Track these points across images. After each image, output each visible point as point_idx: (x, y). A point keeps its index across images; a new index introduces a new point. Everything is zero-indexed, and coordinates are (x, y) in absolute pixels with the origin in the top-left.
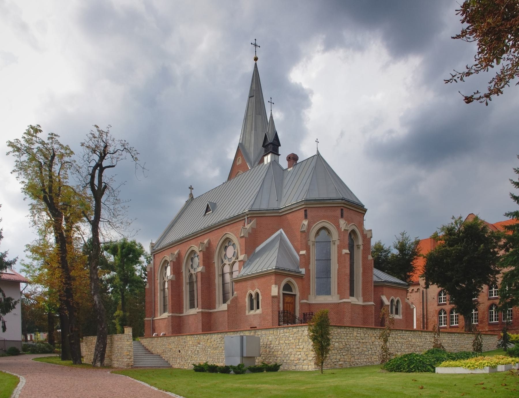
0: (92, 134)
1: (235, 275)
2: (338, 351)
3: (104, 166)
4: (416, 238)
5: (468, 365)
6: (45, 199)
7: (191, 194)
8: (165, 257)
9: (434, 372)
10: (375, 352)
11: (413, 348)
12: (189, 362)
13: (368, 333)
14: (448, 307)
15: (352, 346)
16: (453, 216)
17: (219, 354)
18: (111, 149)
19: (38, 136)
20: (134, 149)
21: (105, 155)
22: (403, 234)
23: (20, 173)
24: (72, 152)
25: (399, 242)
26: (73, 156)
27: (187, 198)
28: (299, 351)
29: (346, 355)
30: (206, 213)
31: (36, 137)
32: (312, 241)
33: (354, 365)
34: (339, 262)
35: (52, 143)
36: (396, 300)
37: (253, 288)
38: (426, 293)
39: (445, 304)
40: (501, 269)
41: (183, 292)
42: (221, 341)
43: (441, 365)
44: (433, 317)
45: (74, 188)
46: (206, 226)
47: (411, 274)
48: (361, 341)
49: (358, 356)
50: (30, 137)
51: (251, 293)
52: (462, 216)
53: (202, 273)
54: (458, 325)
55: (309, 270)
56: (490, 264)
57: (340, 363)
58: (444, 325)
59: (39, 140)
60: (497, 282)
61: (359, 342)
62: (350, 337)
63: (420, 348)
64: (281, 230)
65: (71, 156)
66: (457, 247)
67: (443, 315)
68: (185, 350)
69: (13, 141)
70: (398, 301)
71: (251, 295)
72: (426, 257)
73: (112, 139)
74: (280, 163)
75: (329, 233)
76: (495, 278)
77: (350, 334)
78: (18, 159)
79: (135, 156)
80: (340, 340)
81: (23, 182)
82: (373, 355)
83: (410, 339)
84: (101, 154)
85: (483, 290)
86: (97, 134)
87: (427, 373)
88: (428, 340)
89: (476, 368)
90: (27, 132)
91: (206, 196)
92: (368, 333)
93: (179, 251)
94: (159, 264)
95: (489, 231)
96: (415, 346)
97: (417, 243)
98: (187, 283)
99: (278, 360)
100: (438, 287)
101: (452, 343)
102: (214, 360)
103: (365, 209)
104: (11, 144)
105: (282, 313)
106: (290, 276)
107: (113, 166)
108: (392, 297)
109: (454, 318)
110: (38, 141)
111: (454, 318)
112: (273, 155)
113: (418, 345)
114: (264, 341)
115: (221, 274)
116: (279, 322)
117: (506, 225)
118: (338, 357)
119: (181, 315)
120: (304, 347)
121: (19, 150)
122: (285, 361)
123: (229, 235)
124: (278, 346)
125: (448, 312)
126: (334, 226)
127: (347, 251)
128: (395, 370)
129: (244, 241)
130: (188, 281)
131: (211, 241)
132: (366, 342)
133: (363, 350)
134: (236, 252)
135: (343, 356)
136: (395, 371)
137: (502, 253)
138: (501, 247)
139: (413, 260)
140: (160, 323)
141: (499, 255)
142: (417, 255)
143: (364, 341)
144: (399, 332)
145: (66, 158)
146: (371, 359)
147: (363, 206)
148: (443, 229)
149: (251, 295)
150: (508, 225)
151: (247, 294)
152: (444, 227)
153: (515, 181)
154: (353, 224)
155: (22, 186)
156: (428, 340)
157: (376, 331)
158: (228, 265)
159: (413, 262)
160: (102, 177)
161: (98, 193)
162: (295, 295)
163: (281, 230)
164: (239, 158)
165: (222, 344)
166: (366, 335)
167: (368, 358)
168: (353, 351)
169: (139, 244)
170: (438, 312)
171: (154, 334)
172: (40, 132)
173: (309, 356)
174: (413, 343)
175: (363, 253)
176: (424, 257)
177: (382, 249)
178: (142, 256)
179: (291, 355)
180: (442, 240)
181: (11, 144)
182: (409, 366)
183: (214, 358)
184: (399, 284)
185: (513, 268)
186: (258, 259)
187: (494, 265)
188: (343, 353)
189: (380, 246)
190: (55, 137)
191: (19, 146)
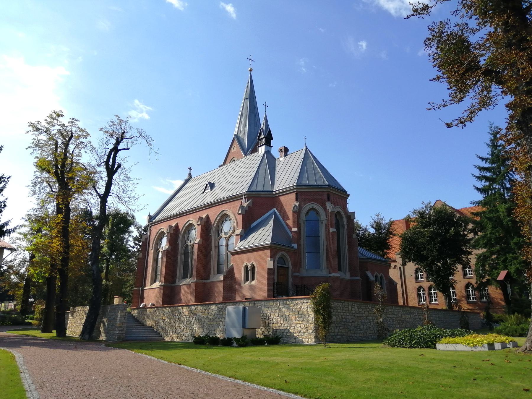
0: (112, 122)
1: (232, 248)
2: (335, 324)
3: (119, 148)
4: (390, 219)
5: (467, 342)
6: (56, 173)
7: (190, 175)
8: (162, 228)
9: (435, 348)
10: (369, 327)
11: (404, 324)
13: (362, 307)
14: (426, 285)
15: (348, 320)
16: (423, 202)
17: (216, 325)
18: (127, 135)
19: (59, 120)
20: (150, 137)
21: (122, 139)
22: (378, 215)
23: (36, 149)
24: (88, 135)
25: (375, 222)
26: (89, 138)
27: (187, 177)
28: (299, 324)
29: (343, 329)
30: (205, 191)
31: (57, 120)
32: (303, 220)
33: (351, 339)
34: (327, 239)
35: (72, 126)
37: (249, 260)
39: (423, 282)
40: (472, 250)
41: (177, 262)
42: (219, 312)
43: (441, 341)
44: (412, 293)
45: (85, 165)
46: (205, 202)
47: (388, 251)
48: (356, 315)
49: (354, 330)
50: (51, 120)
51: (246, 265)
52: (431, 202)
54: (437, 302)
55: (300, 245)
56: (462, 246)
57: (338, 337)
58: (435, 301)
59: (60, 123)
60: (470, 263)
61: (354, 316)
62: (346, 311)
63: (410, 325)
64: (275, 209)
65: (87, 138)
66: (429, 229)
67: (421, 292)
69: (34, 122)
71: (247, 267)
72: (402, 237)
73: (129, 127)
74: (272, 153)
75: (317, 213)
76: (468, 258)
77: (346, 308)
78: (36, 138)
79: (150, 143)
80: (337, 313)
81: (37, 157)
82: (368, 330)
83: (400, 314)
84: (118, 138)
85: (458, 269)
86: (117, 122)
87: (428, 349)
88: (417, 316)
89: (476, 345)
90: (49, 116)
91: (204, 176)
92: (362, 307)
94: (155, 235)
95: (457, 216)
96: (405, 322)
97: (391, 223)
99: (277, 333)
101: (439, 321)
102: (210, 332)
103: (348, 194)
104: (31, 125)
105: (276, 285)
106: (283, 251)
107: (128, 149)
108: (376, 273)
109: (433, 295)
110: (59, 123)
111: (422, 296)
112: (267, 146)
113: (408, 321)
114: (263, 313)
116: (274, 293)
117: (473, 212)
118: (336, 331)
119: (173, 285)
120: (303, 319)
121: (38, 129)
122: (285, 333)
123: (227, 211)
124: (277, 318)
125: (426, 289)
126: (321, 207)
127: (335, 230)
128: (397, 345)
129: (242, 217)
130: (183, 251)
131: (210, 216)
132: (361, 317)
133: (358, 324)
134: (233, 226)
135: (341, 329)
136: (398, 347)
137: (471, 235)
138: (471, 231)
139: (388, 238)
140: (150, 293)
141: (468, 238)
142: (392, 234)
143: (358, 315)
144: (389, 308)
145: (517, 175)
146: (366, 334)
147: (346, 192)
148: (415, 212)
149: (247, 267)
150: (475, 212)
151: (243, 265)
152: (415, 211)
153: (476, 175)
154: (338, 206)
155: (36, 160)
156: (417, 316)
157: (368, 306)
158: (225, 239)
159: (389, 241)
160: (117, 158)
161: (111, 171)
162: (288, 268)
163: (275, 209)
164: (234, 147)
165: (220, 315)
166: (360, 310)
167: (363, 333)
168: (349, 325)
169: (132, 215)
171: (142, 304)
172: (62, 116)
173: (309, 329)
174: (403, 319)
175: (348, 232)
176: (400, 237)
177: (361, 228)
178: (132, 226)
179: (291, 327)
180: (414, 222)
181: (31, 125)
182: (410, 342)
183: (211, 329)
184: (377, 260)
185: (484, 250)
186: (254, 234)
187: (465, 246)
188: (340, 326)
190: (75, 121)
191: (39, 127)
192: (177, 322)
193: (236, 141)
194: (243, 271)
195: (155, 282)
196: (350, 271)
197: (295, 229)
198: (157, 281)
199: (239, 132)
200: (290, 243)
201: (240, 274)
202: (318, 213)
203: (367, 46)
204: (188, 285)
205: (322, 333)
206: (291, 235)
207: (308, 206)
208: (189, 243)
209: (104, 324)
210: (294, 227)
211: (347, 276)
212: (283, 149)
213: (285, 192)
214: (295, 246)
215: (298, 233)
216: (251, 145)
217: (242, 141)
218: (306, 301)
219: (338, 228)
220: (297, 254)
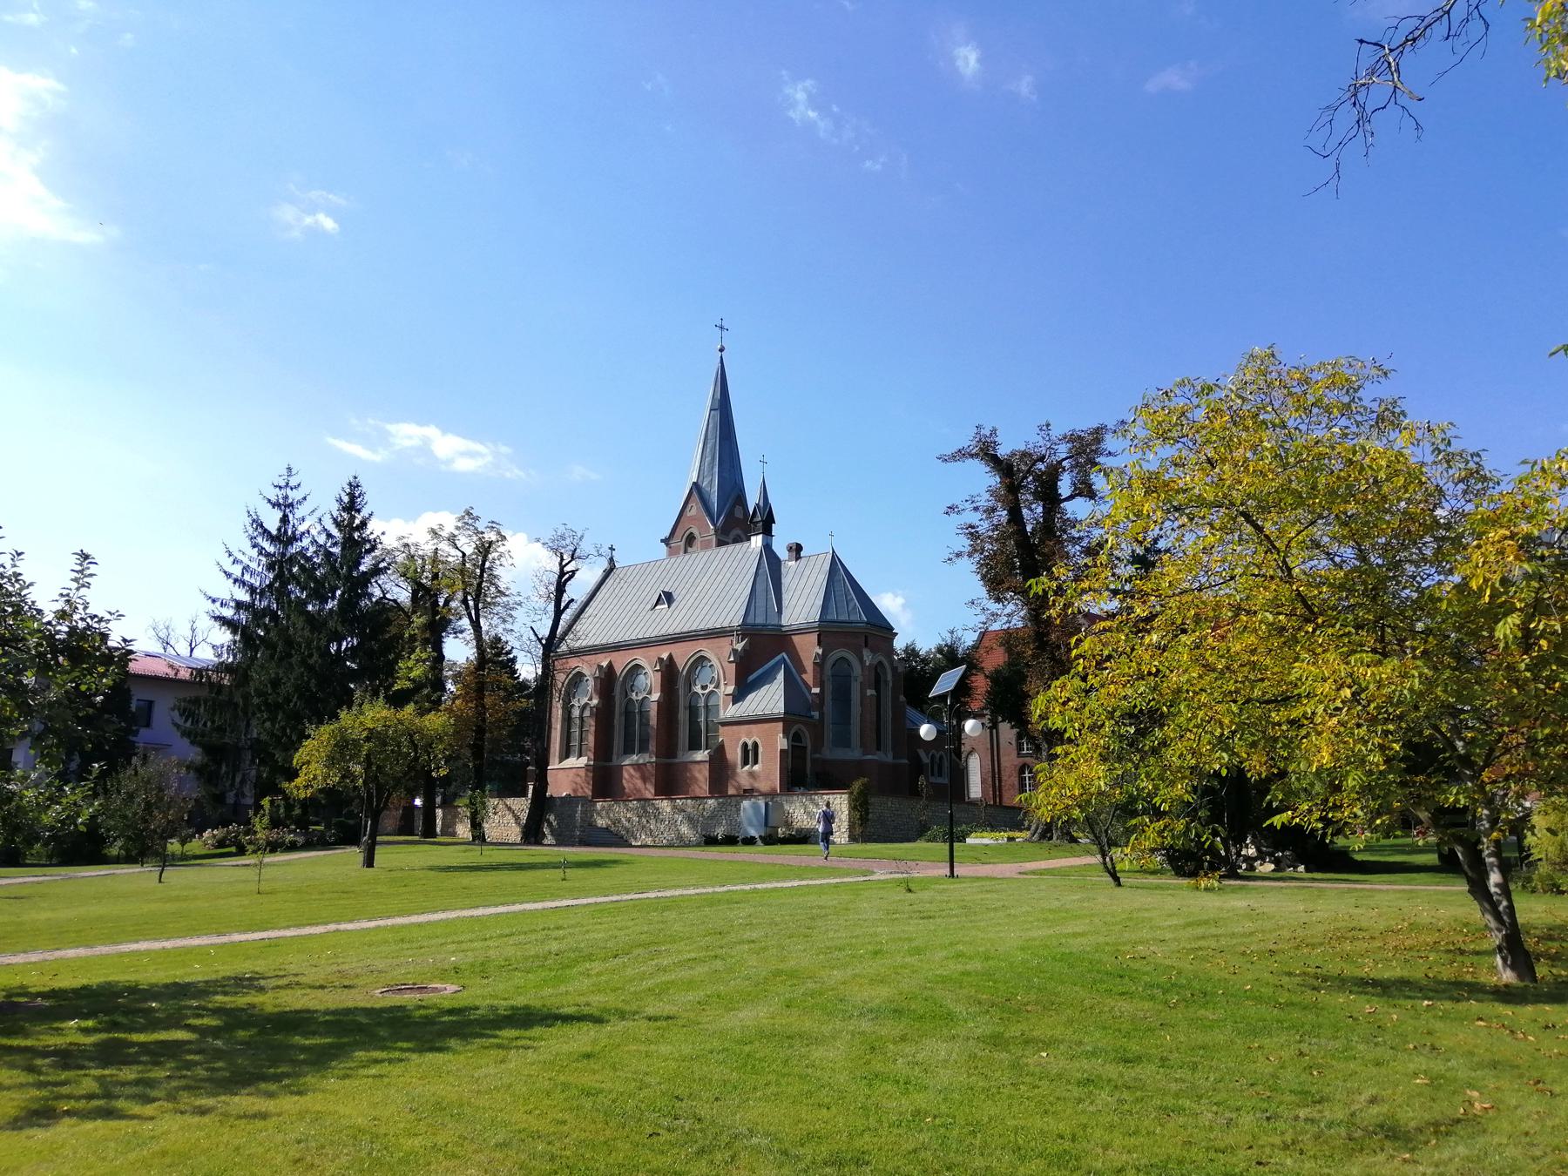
7: (611, 560)
27: (605, 565)
30: (656, 605)
34: (862, 704)
36: (938, 756)
37: (749, 735)
44: (1010, 777)
64: (784, 654)
67: (1027, 775)
70: (941, 758)
71: (745, 745)
98: (620, 715)
100: (1012, 727)
109: (1027, 782)
119: (607, 764)
127: (874, 692)
130: (623, 710)
149: (745, 745)
162: (806, 747)
163: (784, 654)
170: (1018, 768)
186: (753, 694)
189: (914, 650)
192: (653, 822)
193: (695, 495)
194: (739, 751)
195: (567, 757)
196: (893, 749)
197: (816, 690)
198: (572, 752)
199: (701, 478)
200: (809, 710)
201: (734, 754)
202: (849, 664)
203: (979, 60)
204: (637, 767)
205: (858, 830)
206: (810, 698)
207: (837, 654)
208: (634, 696)
209: (550, 824)
210: (815, 686)
211: (889, 758)
212: (794, 547)
213: (801, 631)
214: (816, 714)
215: (821, 695)
216: (725, 505)
217: (706, 496)
218: (839, 796)
219: (878, 689)
220: (817, 728)
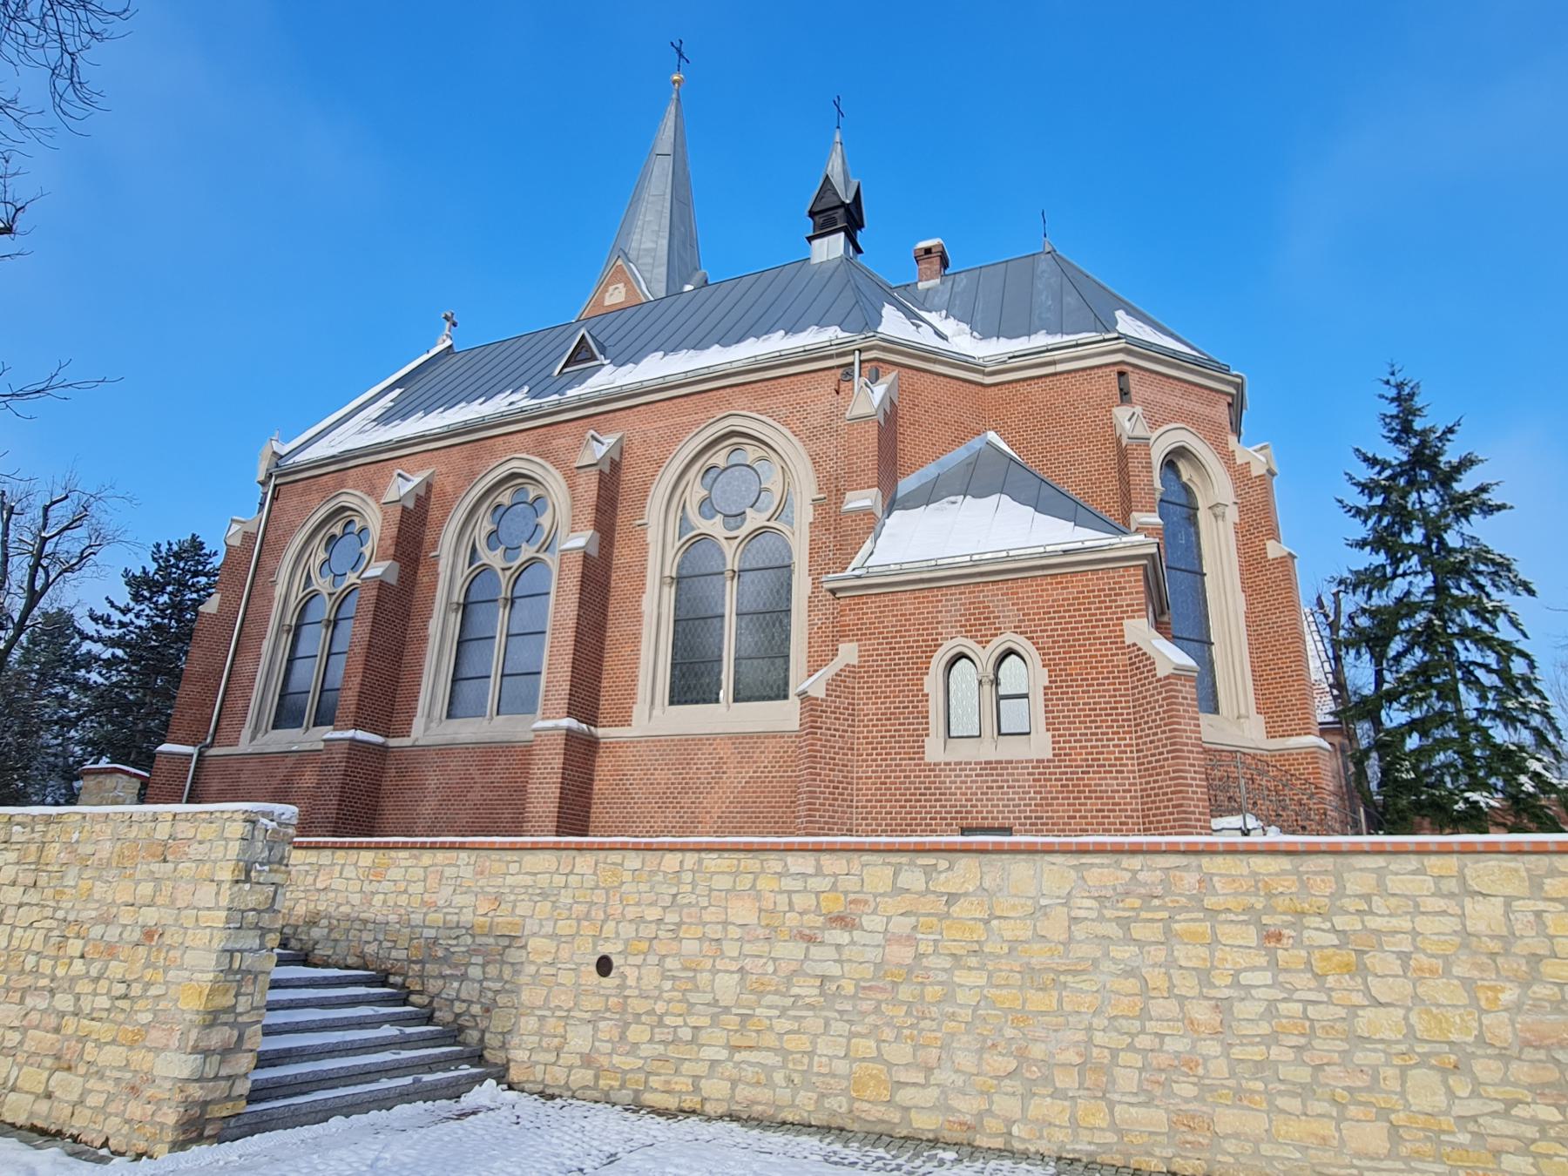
12: (714, 1063)
34: (1249, 587)
38: (998, 850)
53: (382, 584)
68: (670, 963)
93: (620, 447)
115: (461, 601)
119: (393, 742)
